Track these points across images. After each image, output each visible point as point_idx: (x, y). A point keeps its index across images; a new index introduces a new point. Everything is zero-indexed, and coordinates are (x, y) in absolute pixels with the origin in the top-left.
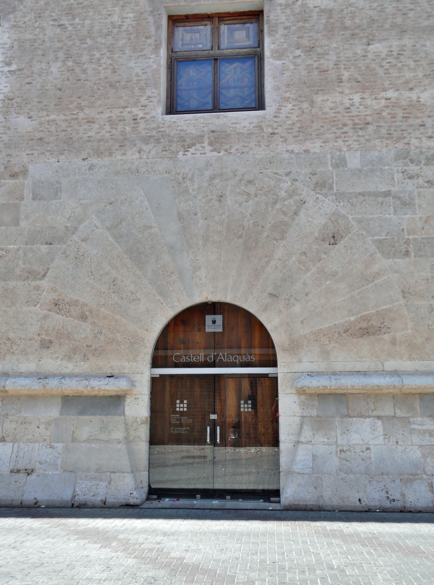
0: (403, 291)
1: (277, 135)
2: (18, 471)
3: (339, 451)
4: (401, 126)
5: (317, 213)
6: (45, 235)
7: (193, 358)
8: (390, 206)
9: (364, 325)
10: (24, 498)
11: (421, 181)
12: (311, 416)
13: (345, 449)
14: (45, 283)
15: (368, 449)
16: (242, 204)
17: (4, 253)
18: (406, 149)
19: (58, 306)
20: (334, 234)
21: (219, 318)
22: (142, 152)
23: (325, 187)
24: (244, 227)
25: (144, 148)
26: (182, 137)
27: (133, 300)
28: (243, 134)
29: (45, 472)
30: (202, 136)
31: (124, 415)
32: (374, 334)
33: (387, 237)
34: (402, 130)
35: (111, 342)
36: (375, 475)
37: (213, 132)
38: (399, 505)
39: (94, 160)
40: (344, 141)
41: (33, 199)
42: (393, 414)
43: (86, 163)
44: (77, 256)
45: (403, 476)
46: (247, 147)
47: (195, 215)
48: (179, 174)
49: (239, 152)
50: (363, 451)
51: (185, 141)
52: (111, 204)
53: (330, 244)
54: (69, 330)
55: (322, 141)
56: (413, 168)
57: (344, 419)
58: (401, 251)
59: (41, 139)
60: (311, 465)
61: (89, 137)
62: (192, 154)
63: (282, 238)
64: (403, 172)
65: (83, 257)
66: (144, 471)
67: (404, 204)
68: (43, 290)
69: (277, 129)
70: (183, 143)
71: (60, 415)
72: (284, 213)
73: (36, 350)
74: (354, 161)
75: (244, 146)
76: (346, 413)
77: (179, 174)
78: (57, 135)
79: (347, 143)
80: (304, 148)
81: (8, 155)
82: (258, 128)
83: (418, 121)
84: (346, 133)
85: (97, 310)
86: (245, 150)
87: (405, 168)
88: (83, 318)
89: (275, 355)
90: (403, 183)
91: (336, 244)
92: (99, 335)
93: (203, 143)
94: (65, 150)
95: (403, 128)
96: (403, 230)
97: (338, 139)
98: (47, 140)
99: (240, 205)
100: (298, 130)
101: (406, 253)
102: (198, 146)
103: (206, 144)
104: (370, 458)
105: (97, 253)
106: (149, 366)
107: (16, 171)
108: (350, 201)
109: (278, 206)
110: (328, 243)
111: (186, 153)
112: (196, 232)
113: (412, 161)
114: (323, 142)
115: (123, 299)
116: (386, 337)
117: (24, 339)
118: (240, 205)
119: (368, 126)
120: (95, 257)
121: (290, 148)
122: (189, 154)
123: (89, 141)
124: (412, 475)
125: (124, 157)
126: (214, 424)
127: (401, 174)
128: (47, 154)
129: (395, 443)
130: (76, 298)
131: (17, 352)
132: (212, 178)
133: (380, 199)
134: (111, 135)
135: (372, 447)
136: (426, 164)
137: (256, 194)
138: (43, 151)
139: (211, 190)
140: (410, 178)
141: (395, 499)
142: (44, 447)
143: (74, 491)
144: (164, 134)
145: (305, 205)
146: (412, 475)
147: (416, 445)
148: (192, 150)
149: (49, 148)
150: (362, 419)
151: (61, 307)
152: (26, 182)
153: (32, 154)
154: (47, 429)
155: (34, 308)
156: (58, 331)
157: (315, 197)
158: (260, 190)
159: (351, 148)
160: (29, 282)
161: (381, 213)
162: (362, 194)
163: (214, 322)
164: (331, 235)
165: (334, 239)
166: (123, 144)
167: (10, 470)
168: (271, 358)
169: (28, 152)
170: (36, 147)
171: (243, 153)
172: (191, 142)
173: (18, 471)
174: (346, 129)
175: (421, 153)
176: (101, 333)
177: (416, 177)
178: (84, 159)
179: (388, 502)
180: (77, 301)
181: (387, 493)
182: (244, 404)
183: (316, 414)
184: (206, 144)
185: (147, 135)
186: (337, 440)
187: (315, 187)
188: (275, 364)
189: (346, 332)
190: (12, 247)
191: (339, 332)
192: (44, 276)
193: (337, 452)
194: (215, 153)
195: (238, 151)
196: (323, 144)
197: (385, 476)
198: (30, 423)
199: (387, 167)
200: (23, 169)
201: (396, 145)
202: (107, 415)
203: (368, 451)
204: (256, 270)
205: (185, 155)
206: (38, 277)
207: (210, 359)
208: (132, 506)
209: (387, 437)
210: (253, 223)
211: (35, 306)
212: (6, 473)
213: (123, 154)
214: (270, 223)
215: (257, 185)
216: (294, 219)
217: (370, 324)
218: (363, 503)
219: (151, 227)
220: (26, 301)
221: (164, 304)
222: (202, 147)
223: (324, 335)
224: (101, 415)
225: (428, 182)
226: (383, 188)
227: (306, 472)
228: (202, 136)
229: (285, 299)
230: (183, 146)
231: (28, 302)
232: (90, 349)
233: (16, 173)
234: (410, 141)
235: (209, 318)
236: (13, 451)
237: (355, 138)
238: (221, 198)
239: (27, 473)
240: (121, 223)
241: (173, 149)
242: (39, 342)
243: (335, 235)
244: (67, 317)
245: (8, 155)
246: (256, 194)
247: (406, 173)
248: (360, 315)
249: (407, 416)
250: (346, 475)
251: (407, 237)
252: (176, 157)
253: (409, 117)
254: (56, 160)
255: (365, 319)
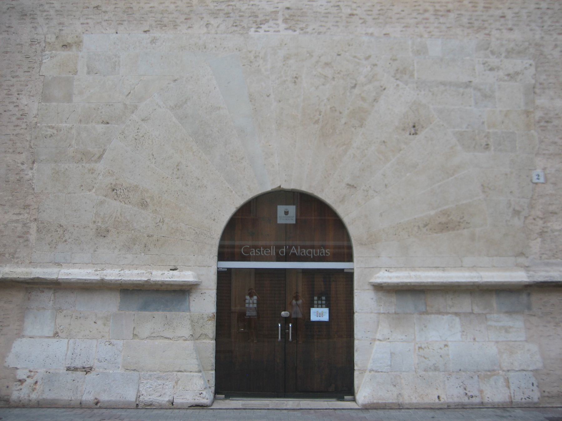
0: (482, 185)
1: (355, 16)
2: (76, 369)
3: (417, 348)
4: (482, 15)
5: (396, 102)
6: (101, 112)
7: (263, 251)
8: (470, 97)
9: (443, 219)
10: (84, 398)
11: (501, 73)
12: (388, 313)
13: (423, 346)
14: (100, 166)
15: (446, 345)
16: (318, 87)
17: (55, 132)
18: (487, 40)
19: (115, 191)
20: (415, 123)
21: (292, 209)
22: (210, 26)
23: (405, 74)
24: (320, 112)
25: (212, 22)
26: (254, 12)
27: (199, 186)
28: (320, 13)
29: (105, 371)
30: (276, 12)
31: (189, 310)
32: (453, 229)
33: (467, 130)
34: (483, 21)
35: (174, 232)
36: (453, 372)
37: (288, 8)
38: (476, 400)
39: (156, 33)
40: (425, 27)
41: (88, 73)
42: (471, 311)
43: (147, 35)
44: (136, 137)
45: (480, 373)
46: (324, 26)
47: (268, 96)
48: (250, 52)
49: (316, 32)
50: (441, 348)
51: (257, 16)
52: (175, 80)
53: (410, 134)
54: (128, 218)
55: (403, 25)
56: (494, 61)
57: (423, 316)
58: (481, 145)
59: (97, 7)
60: (389, 363)
61: (151, 7)
62: (265, 31)
63: (361, 126)
64: (484, 64)
65: (143, 138)
66: (212, 370)
67: (485, 96)
68: (99, 174)
69: (356, 10)
70: (255, 19)
71: (119, 310)
72: (363, 99)
73: (91, 239)
74: (436, 48)
75: (321, 26)
76: (424, 310)
77: (250, 52)
78: (116, 4)
79: (428, 30)
80: (384, 32)
81: (60, 24)
82: (336, 8)
83: (499, 13)
84: (427, 19)
85: (159, 197)
86: (322, 29)
87: (486, 59)
88: (144, 205)
89: (350, 248)
90: (483, 75)
91: (416, 134)
92: (161, 224)
93: (276, 20)
94: (123, 21)
95: (484, 18)
96: (483, 123)
97: (418, 25)
98: (104, 9)
99: (317, 88)
100: (378, 12)
101: (486, 147)
102: (271, 23)
103: (280, 22)
104: (448, 355)
105: (159, 135)
106: (216, 258)
107: (69, 42)
108: (431, 90)
109: (356, 91)
110: (408, 133)
111: (258, 30)
112: (269, 115)
113: (493, 53)
114: (404, 27)
115: (187, 185)
116: (465, 232)
117: (77, 227)
118: (317, 88)
119: (450, 14)
120: (157, 139)
121: (370, 30)
122: (262, 31)
123: (151, 12)
124: (489, 371)
125: (190, 31)
126: (286, 320)
127: (482, 66)
128: (104, 24)
129: (472, 340)
130: (135, 184)
131: (70, 240)
132: (287, 58)
133: (461, 90)
134: (176, 7)
135: (449, 344)
136: (506, 57)
137: (334, 78)
138: (99, 21)
139: (285, 70)
140: (491, 69)
141: (473, 395)
142: (103, 344)
143: (139, 391)
144: (234, 7)
145: (385, 91)
146: (489, 371)
147: (493, 341)
148: (265, 27)
149: (106, 18)
150: (440, 316)
151: (118, 193)
152: (80, 54)
153: (87, 24)
154: (105, 325)
155: (89, 193)
156: (115, 218)
157: (395, 84)
158: (338, 73)
159: (432, 35)
160: (83, 164)
161: (462, 104)
162: (443, 84)
163: (286, 213)
164: (411, 125)
165: (415, 129)
166: (189, 17)
167: (66, 369)
168: (346, 251)
169: (82, 21)
170: (92, 16)
171: (319, 33)
172: (263, 18)
173: (76, 369)
174: (427, 15)
175: (502, 45)
176: (163, 222)
177: (496, 70)
178: (145, 32)
179: (466, 398)
180: (137, 186)
181: (465, 389)
182: (317, 300)
183: (393, 311)
184: (280, 22)
185: (216, 8)
186: (415, 337)
187: (395, 74)
188: (349, 258)
189: (425, 225)
190: (64, 125)
191: (419, 227)
192: (100, 157)
193: (415, 349)
194: (290, 32)
195: (314, 31)
196: (404, 29)
197: (463, 373)
198: (86, 318)
199: (468, 58)
200: (77, 39)
201: (477, 36)
202: (170, 311)
203: (446, 348)
204: (333, 158)
205: (257, 31)
206: (93, 159)
207: (282, 253)
208: (202, 406)
209: (465, 333)
210: (331, 108)
211: (90, 190)
212: (61, 372)
213: (189, 27)
214: (348, 109)
215: (335, 68)
216: (373, 106)
217: (449, 218)
218: (442, 400)
219: (219, 108)
220: (80, 185)
221: (234, 192)
222: (277, 24)
223: (403, 229)
224: (163, 311)
225: (508, 75)
226: (465, 79)
227: (384, 370)
228: (276, 12)
229: (364, 190)
230: (255, 22)
231: (82, 186)
232: (151, 239)
233: (69, 44)
234: (490, 32)
235: (281, 209)
236: (68, 348)
237: (436, 25)
238: (296, 79)
239: (85, 371)
240: (186, 102)
241: (244, 24)
242: (94, 230)
243: (416, 125)
244: (125, 203)
245: (60, 24)
246: (334, 78)
247: (487, 65)
248: (440, 209)
249: (484, 312)
250: (424, 373)
251: (487, 130)
252: (247, 33)
253: (490, 8)
254: (114, 31)
255: (445, 213)
